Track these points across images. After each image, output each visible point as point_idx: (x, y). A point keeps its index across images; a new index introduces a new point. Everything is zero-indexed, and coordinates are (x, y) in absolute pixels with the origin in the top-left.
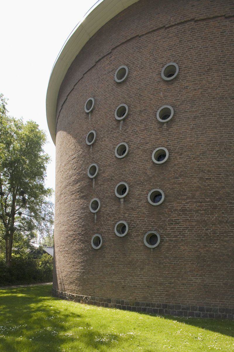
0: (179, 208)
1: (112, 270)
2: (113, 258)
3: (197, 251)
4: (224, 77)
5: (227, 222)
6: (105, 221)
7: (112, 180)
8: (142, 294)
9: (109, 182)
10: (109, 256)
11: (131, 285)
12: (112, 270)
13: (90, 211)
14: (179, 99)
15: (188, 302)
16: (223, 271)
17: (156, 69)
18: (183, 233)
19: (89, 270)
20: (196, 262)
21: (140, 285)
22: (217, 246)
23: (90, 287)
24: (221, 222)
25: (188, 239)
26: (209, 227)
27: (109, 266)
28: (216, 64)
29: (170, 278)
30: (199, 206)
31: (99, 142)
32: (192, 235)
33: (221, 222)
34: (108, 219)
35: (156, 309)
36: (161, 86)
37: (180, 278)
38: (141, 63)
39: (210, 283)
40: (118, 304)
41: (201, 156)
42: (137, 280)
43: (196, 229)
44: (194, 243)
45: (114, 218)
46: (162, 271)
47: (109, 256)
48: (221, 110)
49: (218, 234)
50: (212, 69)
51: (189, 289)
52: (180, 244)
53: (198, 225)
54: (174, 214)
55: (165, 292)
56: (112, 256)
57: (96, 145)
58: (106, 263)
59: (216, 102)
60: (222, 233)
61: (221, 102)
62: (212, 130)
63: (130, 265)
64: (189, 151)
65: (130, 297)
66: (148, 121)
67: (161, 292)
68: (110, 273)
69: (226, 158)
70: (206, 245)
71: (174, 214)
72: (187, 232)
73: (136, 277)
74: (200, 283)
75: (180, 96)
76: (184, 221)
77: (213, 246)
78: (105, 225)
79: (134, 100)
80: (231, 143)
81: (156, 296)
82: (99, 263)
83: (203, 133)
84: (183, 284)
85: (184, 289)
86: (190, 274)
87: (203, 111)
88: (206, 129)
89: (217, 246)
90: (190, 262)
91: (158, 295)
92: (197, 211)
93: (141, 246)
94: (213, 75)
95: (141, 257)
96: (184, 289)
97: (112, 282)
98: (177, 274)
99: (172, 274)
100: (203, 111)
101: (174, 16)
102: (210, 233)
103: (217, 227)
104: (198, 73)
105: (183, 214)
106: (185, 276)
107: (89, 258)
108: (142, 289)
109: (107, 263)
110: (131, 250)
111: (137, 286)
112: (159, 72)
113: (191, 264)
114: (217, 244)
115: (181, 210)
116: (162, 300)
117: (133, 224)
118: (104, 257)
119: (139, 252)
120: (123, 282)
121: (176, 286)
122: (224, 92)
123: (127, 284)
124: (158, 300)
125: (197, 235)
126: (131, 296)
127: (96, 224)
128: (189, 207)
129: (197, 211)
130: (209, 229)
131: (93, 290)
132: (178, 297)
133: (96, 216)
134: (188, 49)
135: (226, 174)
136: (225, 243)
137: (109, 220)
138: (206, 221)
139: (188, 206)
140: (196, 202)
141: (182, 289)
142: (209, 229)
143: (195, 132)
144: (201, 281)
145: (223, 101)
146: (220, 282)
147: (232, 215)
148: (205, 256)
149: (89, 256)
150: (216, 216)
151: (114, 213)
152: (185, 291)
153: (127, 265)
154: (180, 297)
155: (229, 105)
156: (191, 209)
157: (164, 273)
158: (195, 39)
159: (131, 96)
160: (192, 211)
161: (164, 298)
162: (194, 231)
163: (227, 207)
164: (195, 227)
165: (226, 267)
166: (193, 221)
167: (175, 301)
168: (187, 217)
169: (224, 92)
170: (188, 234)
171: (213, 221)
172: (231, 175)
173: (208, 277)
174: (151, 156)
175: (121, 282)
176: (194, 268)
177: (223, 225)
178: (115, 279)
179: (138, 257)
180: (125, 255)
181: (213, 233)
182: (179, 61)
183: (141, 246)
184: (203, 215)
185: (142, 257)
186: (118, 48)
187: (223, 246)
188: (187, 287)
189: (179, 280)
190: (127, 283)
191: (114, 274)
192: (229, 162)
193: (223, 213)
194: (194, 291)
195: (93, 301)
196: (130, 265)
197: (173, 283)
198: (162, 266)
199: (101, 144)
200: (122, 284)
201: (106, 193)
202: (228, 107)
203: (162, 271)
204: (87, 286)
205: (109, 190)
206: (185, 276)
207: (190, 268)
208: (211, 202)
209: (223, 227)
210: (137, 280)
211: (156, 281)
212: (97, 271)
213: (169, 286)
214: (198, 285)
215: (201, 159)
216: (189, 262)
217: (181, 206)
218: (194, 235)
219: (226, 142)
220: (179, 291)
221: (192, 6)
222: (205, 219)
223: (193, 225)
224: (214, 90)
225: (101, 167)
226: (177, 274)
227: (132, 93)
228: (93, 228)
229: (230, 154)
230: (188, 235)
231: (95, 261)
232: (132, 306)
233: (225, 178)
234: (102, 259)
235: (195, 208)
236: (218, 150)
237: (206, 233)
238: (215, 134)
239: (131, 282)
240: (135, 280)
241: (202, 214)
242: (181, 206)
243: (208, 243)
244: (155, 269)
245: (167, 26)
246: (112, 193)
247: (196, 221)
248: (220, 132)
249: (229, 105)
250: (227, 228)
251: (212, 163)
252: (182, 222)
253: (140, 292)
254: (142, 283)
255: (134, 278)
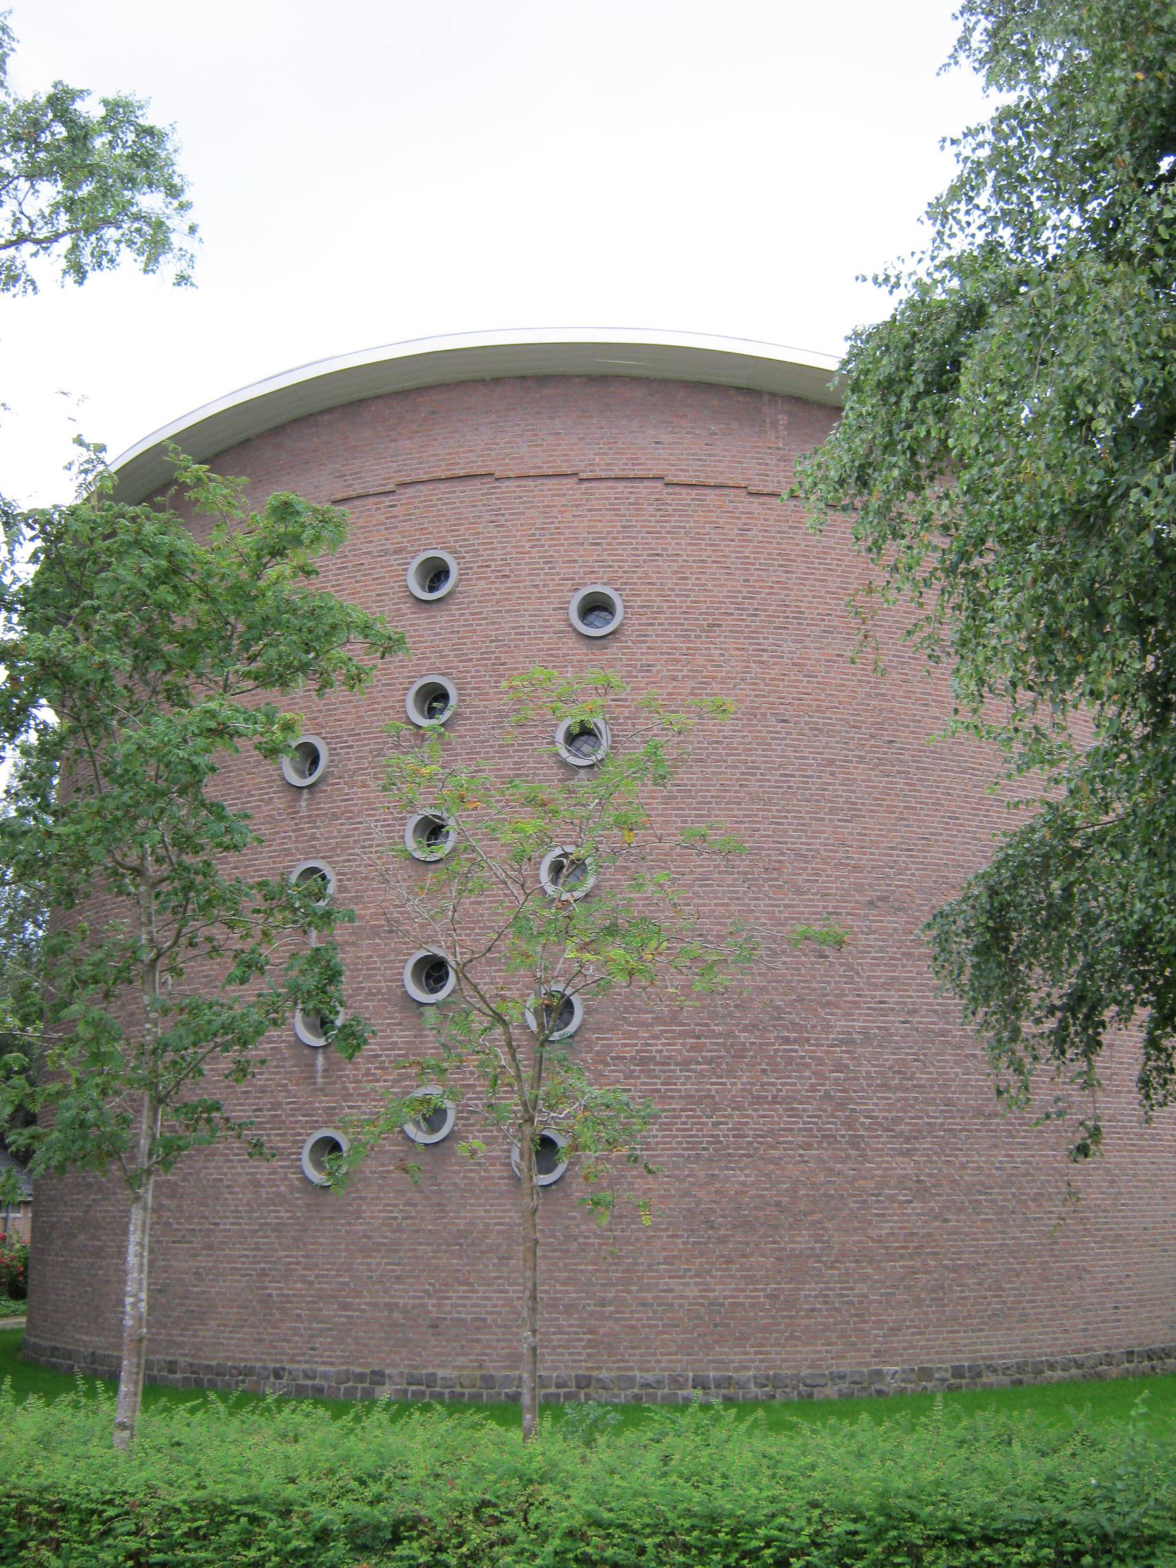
0: (630, 1053)
1: (388, 1264)
2: (395, 1218)
3: (687, 1194)
4: (757, 656)
5: (775, 1100)
6: (360, 1082)
7: (390, 932)
8: (503, 1344)
9: (377, 941)
10: (380, 1211)
11: (462, 1316)
12: (388, 1264)
13: (296, 1035)
14: (626, 700)
15: (658, 1361)
16: (764, 1256)
17: (553, 591)
18: (645, 1137)
19: (291, 1263)
20: (685, 1230)
21: (499, 1313)
22: (746, 1176)
23: (292, 1328)
24: (758, 1100)
25: (658, 1156)
26: (724, 1116)
27: (378, 1251)
28: (731, 614)
29: (602, 1285)
30: (694, 1048)
31: (338, 784)
32: (670, 1143)
33: (758, 1100)
34: (374, 1074)
35: (552, 1395)
36: (570, 649)
37: (635, 1284)
38: (502, 560)
39: (726, 1297)
40: (414, 1388)
41: (696, 888)
42: (488, 1298)
43: (683, 1123)
44: (679, 1169)
45: (399, 1074)
46: (574, 1264)
47: (380, 1211)
48: (751, 750)
49: (750, 1139)
50: (719, 626)
51: (661, 1319)
52: (635, 1173)
53: (690, 1110)
54: (614, 1071)
55: (584, 1333)
56: (391, 1212)
57: (325, 791)
58: (365, 1236)
59: (737, 725)
60: (762, 1136)
61: (750, 725)
62: (729, 810)
63: (461, 1245)
64: (660, 867)
65: (462, 1358)
66: (526, 751)
67: (568, 1333)
68: (382, 1276)
69: (770, 898)
70: (713, 1175)
71: (614, 1071)
72: (654, 1133)
73: (482, 1285)
74: (695, 1298)
75: (628, 690)
76: (643, 1097)
77: (735, 1176)
78: (358, 1095)
79: (477, 671)
80: (783, 854)
81: (555, 1347)
82: (334, 1237)
83: (701, 816)
84: (644, 1305)
85: (648, 1319)
86: (665, 1271)
87: (700, 748)
88: (710, 803)
89: (746, 1176)
90: (666, 1230)
91: (559, 1347)
92: (685, 1064)
93: (500, 1178)
94: (725, 643)
95: (500, 1217)
96: (648, 1319)
97: (391, 1307)
98: (623, 1271)
99: (607, 1271)
100: (700, 748)
101: (606, 454)
102: (726, 1136)
103: (746, 1116)
104: (682, 630)
105: (642, 1071)
106: (649, 1278)
107: (289, 1218)
108: (506, 1327)
109: (369, 1237)
110: (467, 1191)
111: (484, 1320)
112: (564, 603)
113: (669, 1237)
114: (747, 1172)
115: (634, 1058)
116: (574, 1361)
117: (472, 1099)
118: (358, 1214)
119: (494, 1198)
120: (433, 1305)
121: (618, 1312)
122: (756, 696)
123: (450, 1312)
124: (561, 1361)
125: (688, 1142)
126: (465, 1354)
127: (322, 1090)
128: (661, 1051)
129: (685, 1064)
130: (722, 1123)
131: (309, 1342)
132: (626, 1348)
133: (320, 1060)
134: (650, 555)
135: (770, 949)
136: (771, 1167)
137: (378, 1081)
138: (713, 1097)
139: (660, 1047)
140: (682, 1035)
141: (639, 1319)
142: (722, 1123)
143: (678, 809)
144: (700, 1291)
145: (756, 725)
146: (755, 1290)
147: (789, 1077)
148: (713, 1211)
149: (288, 1211)
150: (744, 1080)
151: (399, 1055)
152: (650, 1326)
153: (449, 1245)
154: (632, 1348)
155: (773, 739)
156: (668, 1057)
157: (581, 1271)
158: (668, 533)
159: (466, 654)
160: (669, 1064)
161: (580, 1354)
162: (678, 1130)
163: (776, 1051)
164: (680, 1117)
165: (775, 1243)
166: (672, 1097)
167: (617, 1361)
168: (655, 1084)
169: (756, 696)
170: (659, 1139)
171: (735, 1096)
172: (783, 952)
173: (722, 1276)
174: (538, 869)
175: (424, 1305)
176: (679, 1250)
177: (764, 1110)
178: (401, 1297)
179: (491, 1218)
180: (443, 1211)
181: (734, 1136)
182: (625, 584)
183: (500, 1178)
184: (704, 1076)
185: (504, 1217)
186: (420, 487)
187: (765, 1175)
188: (655, 1312)
189: (630, 1292)
190: (449, 1308)
191: (398, 1277)
192: (780, 912)
193: (764, 1071)
194: (678, 1326)
195: (310, 1383)
196: (461, 1245)
197: (610, 1303)
198: (574, 1247)
199: (347, 794)
200: (430, 1312)
201: (368, 977)
202: (770, 744)
203: (574, 1264)
204: (278, 1328)
205: (379, 969)
206: (649, 1278)
207: (664, 1249)
208: (729, 1034)
209: (764, 1116)
210: (488, 1298)
211: (554, 1299)
212: (328, 1270)
213: (596, 1312)
214: (690, 1304)
215: (696, 894)
216: (660, 1229)
217: (636, 1045)
218: (678, 1143)
219: (769, 849)
220: (632, 1327)
221: (657, 443)
222: (709, 1090)
223: (674, 1110)
224: (729, 689)
225: (349, 880)
226: (623, 1271)
227: (470, 646)
228: (311, 1103)
229: (780, 887)
230: (657, 1143)
231: (318, 1231)
232: (467, 1391)
233: (769, 962)
234: (349, 1224)
235: (679, 1051)
236: (745, 873)
237: (712, 1136)
238: (737, 822)
239: (464, 1306)
240: (478, 1298)
241: (701, 1074)
242: (636, 1045)
243: (721, 1169)
244: (550, 1258)
245: (583, 475)
246: (393, 981)
247: (681, 1097)
248: (749, 816)
249: (773, 739)
250: (776, 1119)
251: (728, 911)
252: (640, 1098)
253: (498, 1340)
254: (505, 1306)
255: (477, 1291)
